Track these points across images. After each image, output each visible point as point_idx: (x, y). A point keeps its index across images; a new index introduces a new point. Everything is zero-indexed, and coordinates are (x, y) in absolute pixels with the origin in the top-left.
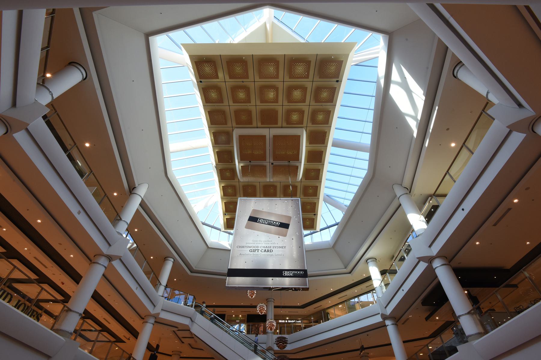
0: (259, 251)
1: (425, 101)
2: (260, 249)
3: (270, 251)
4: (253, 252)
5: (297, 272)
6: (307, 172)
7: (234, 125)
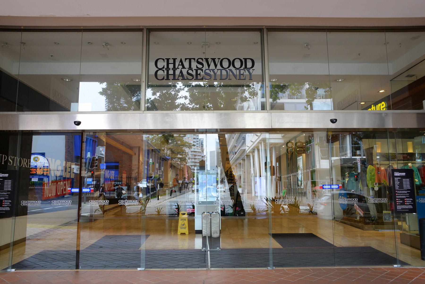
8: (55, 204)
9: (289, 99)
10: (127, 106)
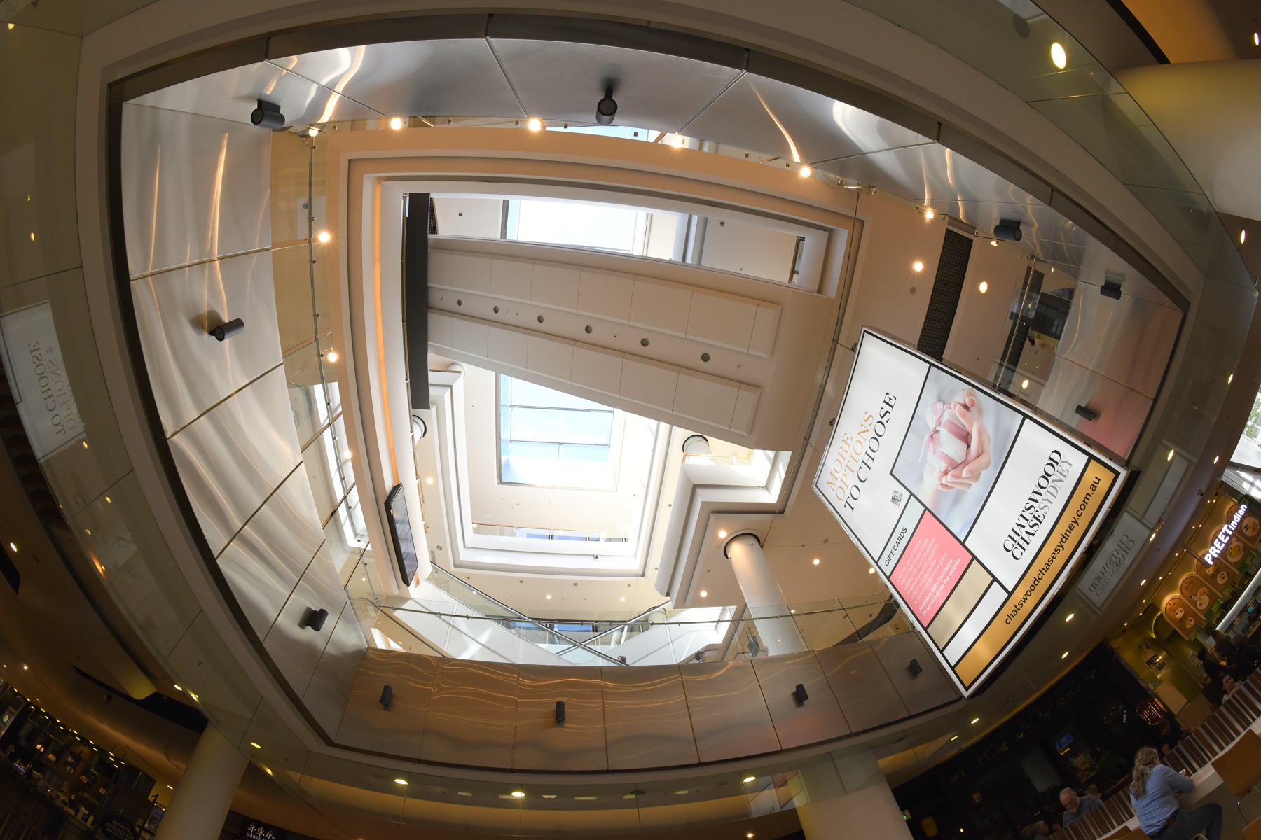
9: (1059, 339)
10: (1019, 738)
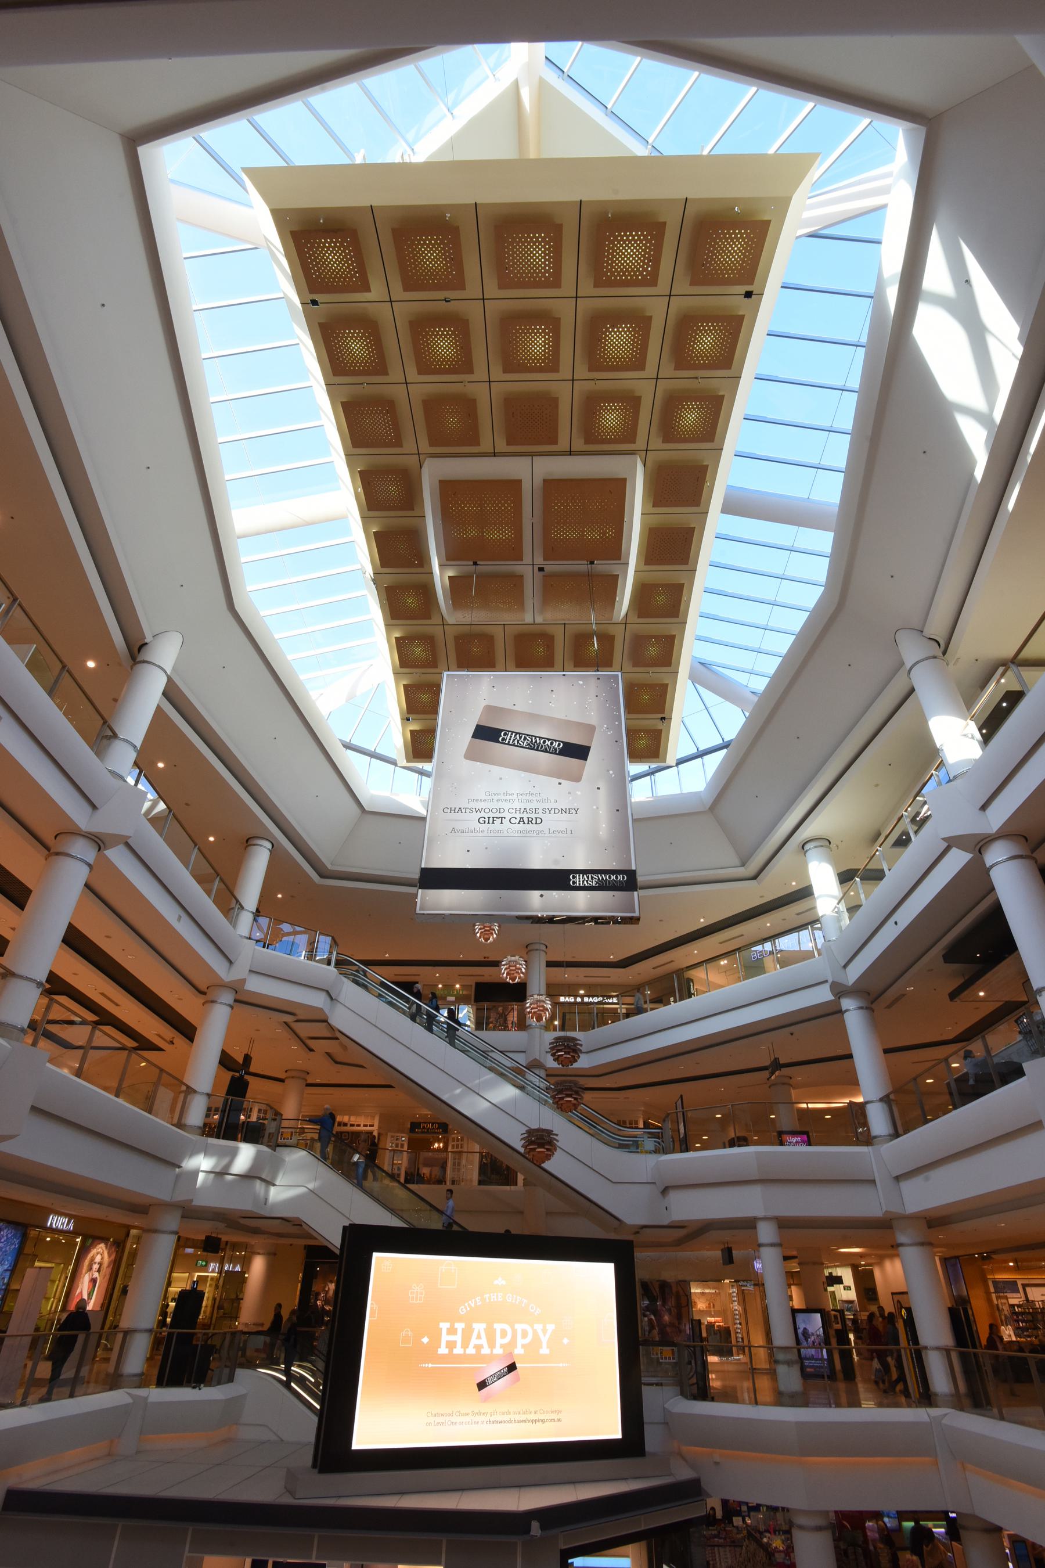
0: (506, 821)
1: (1024, 361)
2: (508, 816)
3: (534, 822)
4: (489, 823)
5: (610, 877)
6: (644, 593)
7: (424, 446)
8: (509, 742)
